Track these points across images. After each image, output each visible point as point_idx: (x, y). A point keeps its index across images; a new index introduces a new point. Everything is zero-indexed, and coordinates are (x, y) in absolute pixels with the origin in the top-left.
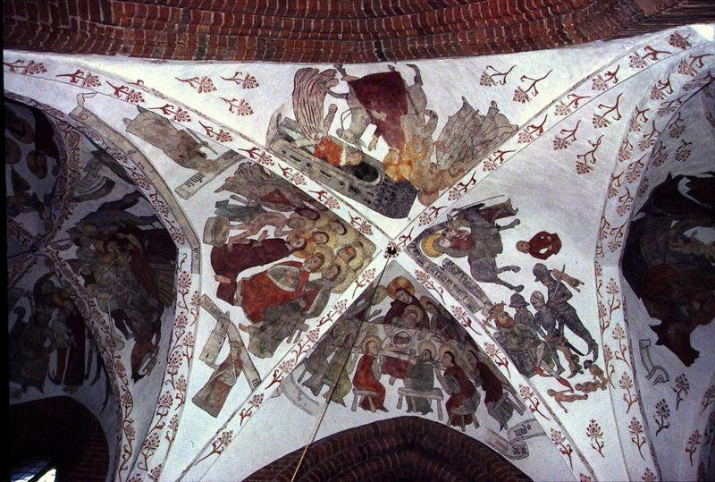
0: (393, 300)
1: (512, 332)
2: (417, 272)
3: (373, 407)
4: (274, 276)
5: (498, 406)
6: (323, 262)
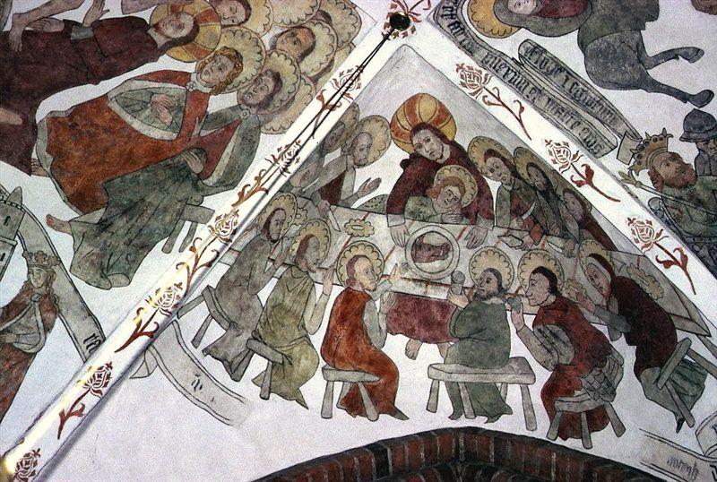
0: (407, 156)
1: (692, 197)
2: (460, 67)
3: (370, 409)
4: (125, 107)
5: (665, 376)
6: (238, 67)
